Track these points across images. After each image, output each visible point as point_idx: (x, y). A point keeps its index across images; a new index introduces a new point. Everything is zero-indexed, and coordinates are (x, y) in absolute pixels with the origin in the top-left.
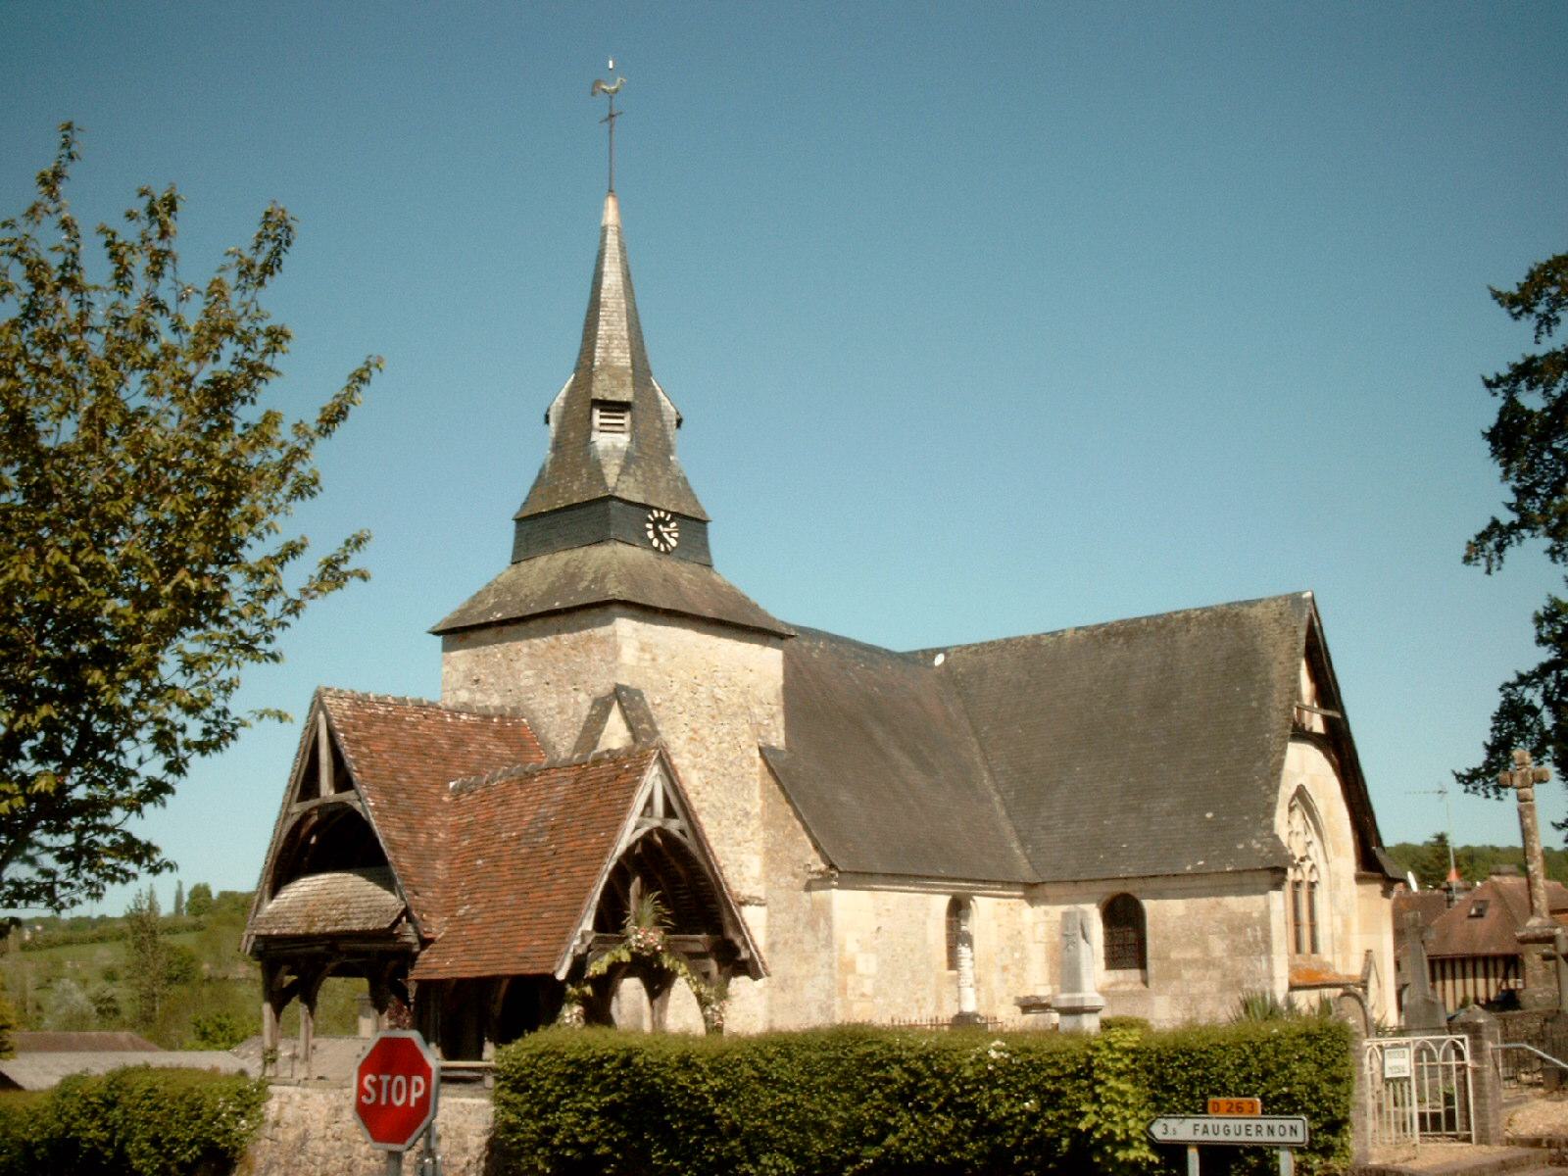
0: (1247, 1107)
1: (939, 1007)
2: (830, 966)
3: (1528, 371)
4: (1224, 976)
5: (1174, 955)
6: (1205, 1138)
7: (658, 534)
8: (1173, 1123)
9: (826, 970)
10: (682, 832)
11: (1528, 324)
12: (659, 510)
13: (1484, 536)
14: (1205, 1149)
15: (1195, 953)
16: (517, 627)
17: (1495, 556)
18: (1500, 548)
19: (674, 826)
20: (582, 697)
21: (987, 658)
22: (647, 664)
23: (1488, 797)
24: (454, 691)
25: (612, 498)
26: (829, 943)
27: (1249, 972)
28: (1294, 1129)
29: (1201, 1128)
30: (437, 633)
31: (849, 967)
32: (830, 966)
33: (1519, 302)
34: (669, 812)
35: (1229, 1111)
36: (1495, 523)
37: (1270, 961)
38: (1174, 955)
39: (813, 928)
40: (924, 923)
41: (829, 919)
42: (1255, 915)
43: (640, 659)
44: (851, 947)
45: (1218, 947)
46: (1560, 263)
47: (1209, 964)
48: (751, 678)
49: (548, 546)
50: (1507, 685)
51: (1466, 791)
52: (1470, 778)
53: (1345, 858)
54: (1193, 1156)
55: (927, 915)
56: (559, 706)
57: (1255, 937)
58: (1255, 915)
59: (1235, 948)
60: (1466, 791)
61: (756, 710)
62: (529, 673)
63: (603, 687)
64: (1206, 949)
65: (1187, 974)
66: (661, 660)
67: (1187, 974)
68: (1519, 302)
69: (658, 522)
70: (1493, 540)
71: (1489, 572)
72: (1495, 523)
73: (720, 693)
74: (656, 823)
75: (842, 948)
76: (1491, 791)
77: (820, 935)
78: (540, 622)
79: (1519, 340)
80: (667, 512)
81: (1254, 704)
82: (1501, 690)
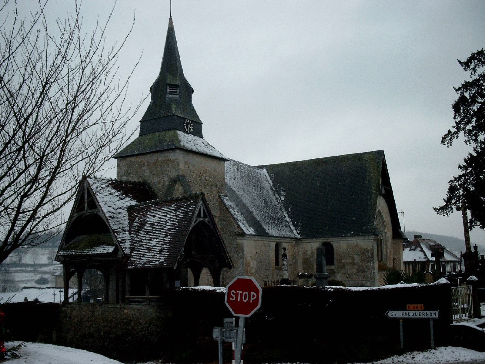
0: (419, 307)
1: (273, 277)
2: (243, 264)
3: (467, 86)
4: (359, 268)
5: (343, 261)
6: (406, 317)
7: (187, 127)
8: (395, 312)
9: (241, 265)
10: (208, 222)
11: (469, 71)
12: (188, 119)
13: (446, 136)
14: (403, 319)
15: (350, 261)
16: (198, 156)
17: (450, 141)
18: (451, 139)
19: (206, 220)
20: (166, 179)
21: (280, 169)
22: (187, 168)
23: (444, 215)
24: (121, 176)
25: (174, 115)
26: (242, 257)
27: (367, 266)
28: (434, 314)
29: (404, 314)
30: (115, 158)
31: (248, 265)
32: (243, 264)
33: (466, 65)
34: (205, 216)
35: (414, 308)
36: (450, 132)
37: (373, 263)
38: (343, 261)
39: (237, 252)
40: (269, 251)
41: (242, 250)
42: (369, 249)
43: (185, 167)
44: (249, 258)
45: (357, 259)
46: (480, 53)
47: (354, 263)
48: (215, 174)
49: (154, 131)
50: (451, 181)
51: (438, 214)
52: (437, 210)
53: (389, 234)
54: (431, 322)
55: (269, 248)
56: (158, 181)
57: (369, 256)
58: (369, 249)
59: (362, 259)
60: (438, 214)
61: (218, 183)
62: (147, 171)
63: (173, 174)
64: (353, 259)
65: (348, 267)
66: (191, 167)
67: (348, 267)
68: (466, 65)
69: (188, 123)
70: (448, 138)
71: (448, 147)
72: (450, 132)
73: (207, 178)
74: (201, 219)
75: (246, 258)
76: (445, 214)
77: (240, 255)
78: (151, 155)
79: (467, 76)
80: (190, 120)
81: (367, 185)
82: (449, 183)
